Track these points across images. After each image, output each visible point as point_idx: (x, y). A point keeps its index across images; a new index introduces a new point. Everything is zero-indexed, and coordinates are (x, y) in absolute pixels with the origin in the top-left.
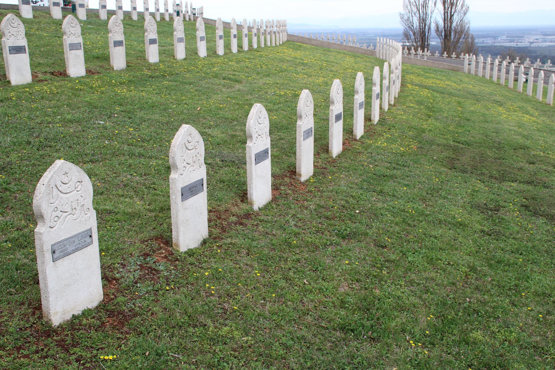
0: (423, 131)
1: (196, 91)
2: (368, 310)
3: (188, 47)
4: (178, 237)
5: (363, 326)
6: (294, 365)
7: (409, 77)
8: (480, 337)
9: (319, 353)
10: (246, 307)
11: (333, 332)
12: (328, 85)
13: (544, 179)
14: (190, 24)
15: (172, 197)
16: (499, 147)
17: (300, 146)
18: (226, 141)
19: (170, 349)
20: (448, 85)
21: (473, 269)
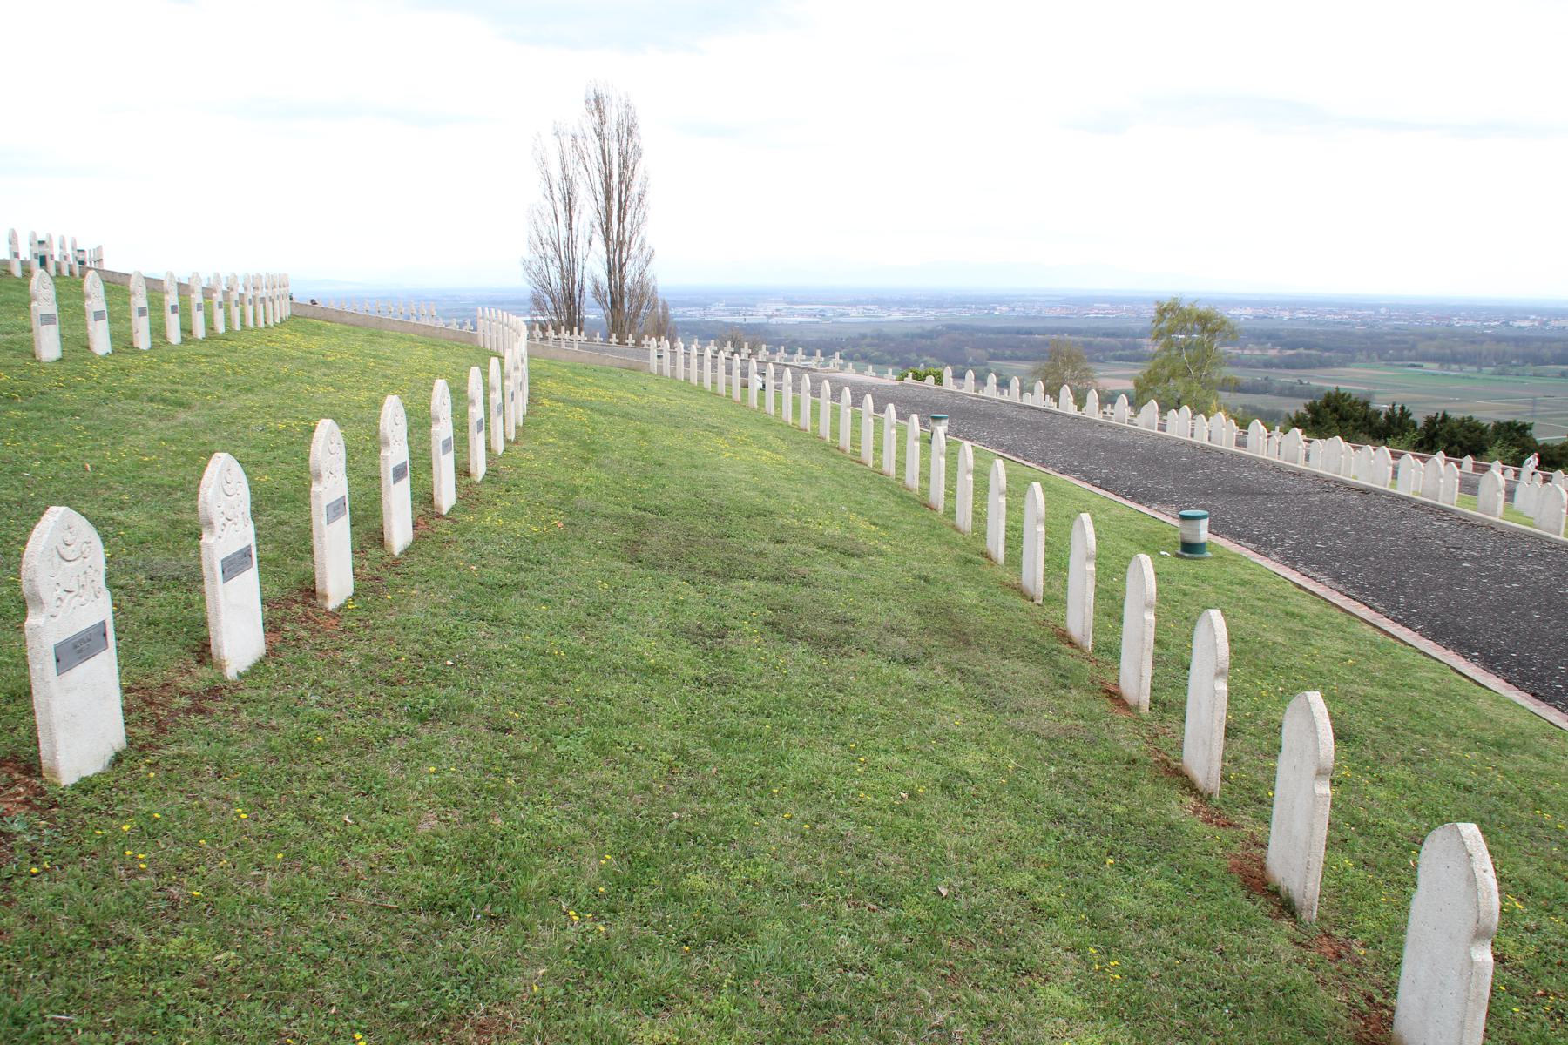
0: (575, 491)
1: (87, 428)
2: (482, 861)
3: (67, 333)
4: (54, 755)
5: (473, 894)
6: (333, 995)
7: (545, 385)
8: (703, 884)
9: (387, 963)
10: (219, 890)
11: (412, 916)
13: (801, 570)
14: (70, 284)
15: (35, 668)
16: (720, 514)
17: (321, 537)
18: (159, 535)
19: (47, 1006)
20: (620, 398)
21: (682, 754)
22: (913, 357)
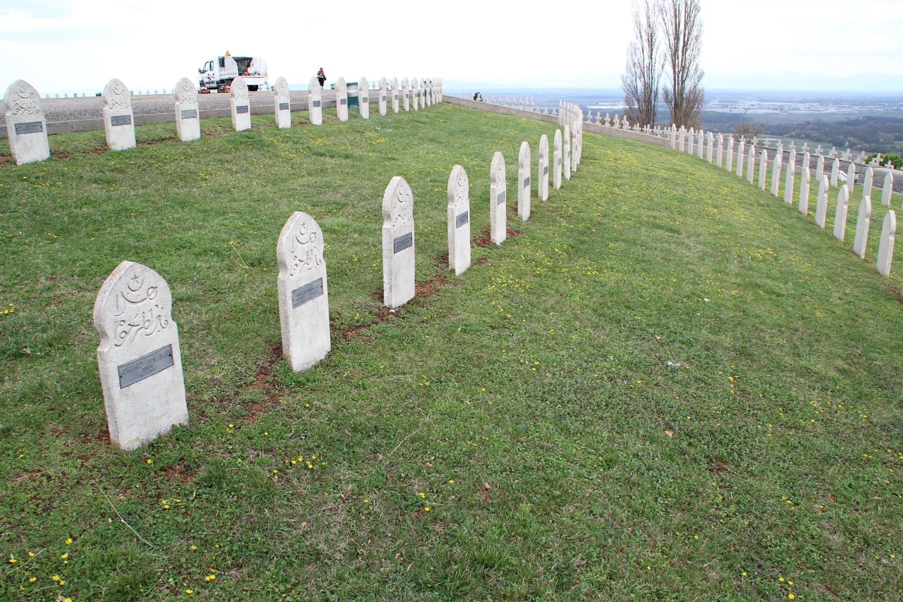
12: (488, 160)
22: (841, 137)
